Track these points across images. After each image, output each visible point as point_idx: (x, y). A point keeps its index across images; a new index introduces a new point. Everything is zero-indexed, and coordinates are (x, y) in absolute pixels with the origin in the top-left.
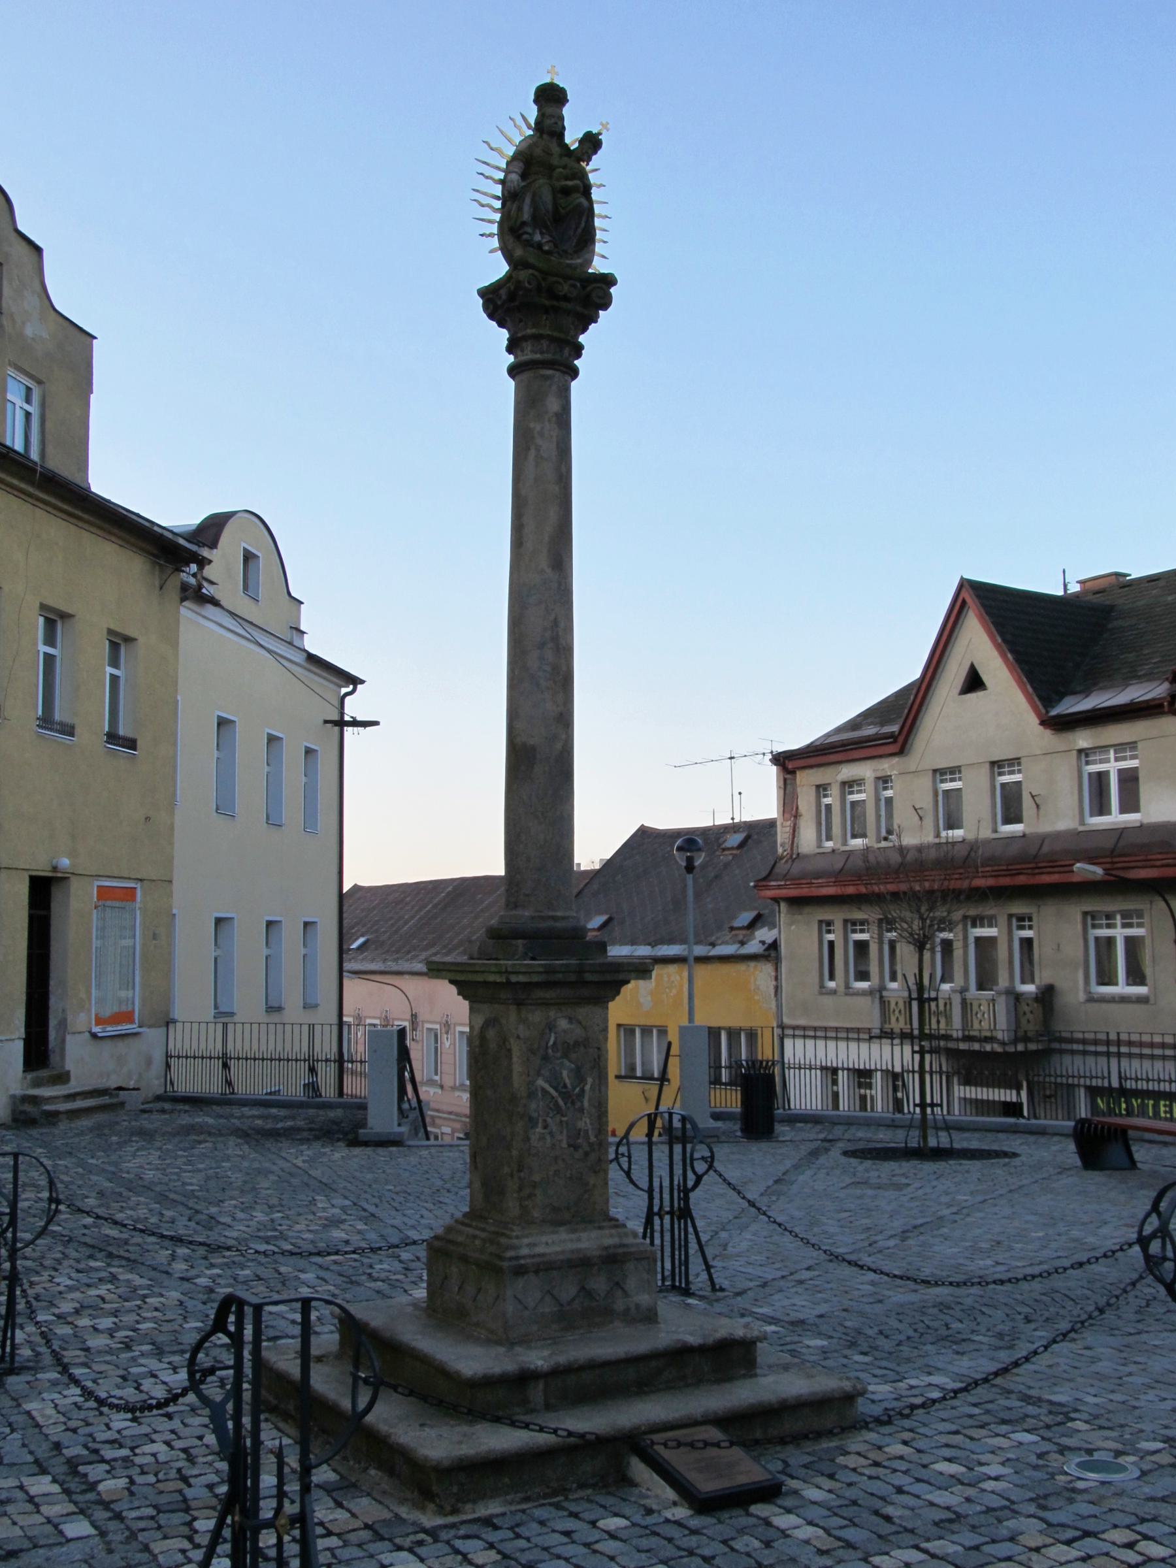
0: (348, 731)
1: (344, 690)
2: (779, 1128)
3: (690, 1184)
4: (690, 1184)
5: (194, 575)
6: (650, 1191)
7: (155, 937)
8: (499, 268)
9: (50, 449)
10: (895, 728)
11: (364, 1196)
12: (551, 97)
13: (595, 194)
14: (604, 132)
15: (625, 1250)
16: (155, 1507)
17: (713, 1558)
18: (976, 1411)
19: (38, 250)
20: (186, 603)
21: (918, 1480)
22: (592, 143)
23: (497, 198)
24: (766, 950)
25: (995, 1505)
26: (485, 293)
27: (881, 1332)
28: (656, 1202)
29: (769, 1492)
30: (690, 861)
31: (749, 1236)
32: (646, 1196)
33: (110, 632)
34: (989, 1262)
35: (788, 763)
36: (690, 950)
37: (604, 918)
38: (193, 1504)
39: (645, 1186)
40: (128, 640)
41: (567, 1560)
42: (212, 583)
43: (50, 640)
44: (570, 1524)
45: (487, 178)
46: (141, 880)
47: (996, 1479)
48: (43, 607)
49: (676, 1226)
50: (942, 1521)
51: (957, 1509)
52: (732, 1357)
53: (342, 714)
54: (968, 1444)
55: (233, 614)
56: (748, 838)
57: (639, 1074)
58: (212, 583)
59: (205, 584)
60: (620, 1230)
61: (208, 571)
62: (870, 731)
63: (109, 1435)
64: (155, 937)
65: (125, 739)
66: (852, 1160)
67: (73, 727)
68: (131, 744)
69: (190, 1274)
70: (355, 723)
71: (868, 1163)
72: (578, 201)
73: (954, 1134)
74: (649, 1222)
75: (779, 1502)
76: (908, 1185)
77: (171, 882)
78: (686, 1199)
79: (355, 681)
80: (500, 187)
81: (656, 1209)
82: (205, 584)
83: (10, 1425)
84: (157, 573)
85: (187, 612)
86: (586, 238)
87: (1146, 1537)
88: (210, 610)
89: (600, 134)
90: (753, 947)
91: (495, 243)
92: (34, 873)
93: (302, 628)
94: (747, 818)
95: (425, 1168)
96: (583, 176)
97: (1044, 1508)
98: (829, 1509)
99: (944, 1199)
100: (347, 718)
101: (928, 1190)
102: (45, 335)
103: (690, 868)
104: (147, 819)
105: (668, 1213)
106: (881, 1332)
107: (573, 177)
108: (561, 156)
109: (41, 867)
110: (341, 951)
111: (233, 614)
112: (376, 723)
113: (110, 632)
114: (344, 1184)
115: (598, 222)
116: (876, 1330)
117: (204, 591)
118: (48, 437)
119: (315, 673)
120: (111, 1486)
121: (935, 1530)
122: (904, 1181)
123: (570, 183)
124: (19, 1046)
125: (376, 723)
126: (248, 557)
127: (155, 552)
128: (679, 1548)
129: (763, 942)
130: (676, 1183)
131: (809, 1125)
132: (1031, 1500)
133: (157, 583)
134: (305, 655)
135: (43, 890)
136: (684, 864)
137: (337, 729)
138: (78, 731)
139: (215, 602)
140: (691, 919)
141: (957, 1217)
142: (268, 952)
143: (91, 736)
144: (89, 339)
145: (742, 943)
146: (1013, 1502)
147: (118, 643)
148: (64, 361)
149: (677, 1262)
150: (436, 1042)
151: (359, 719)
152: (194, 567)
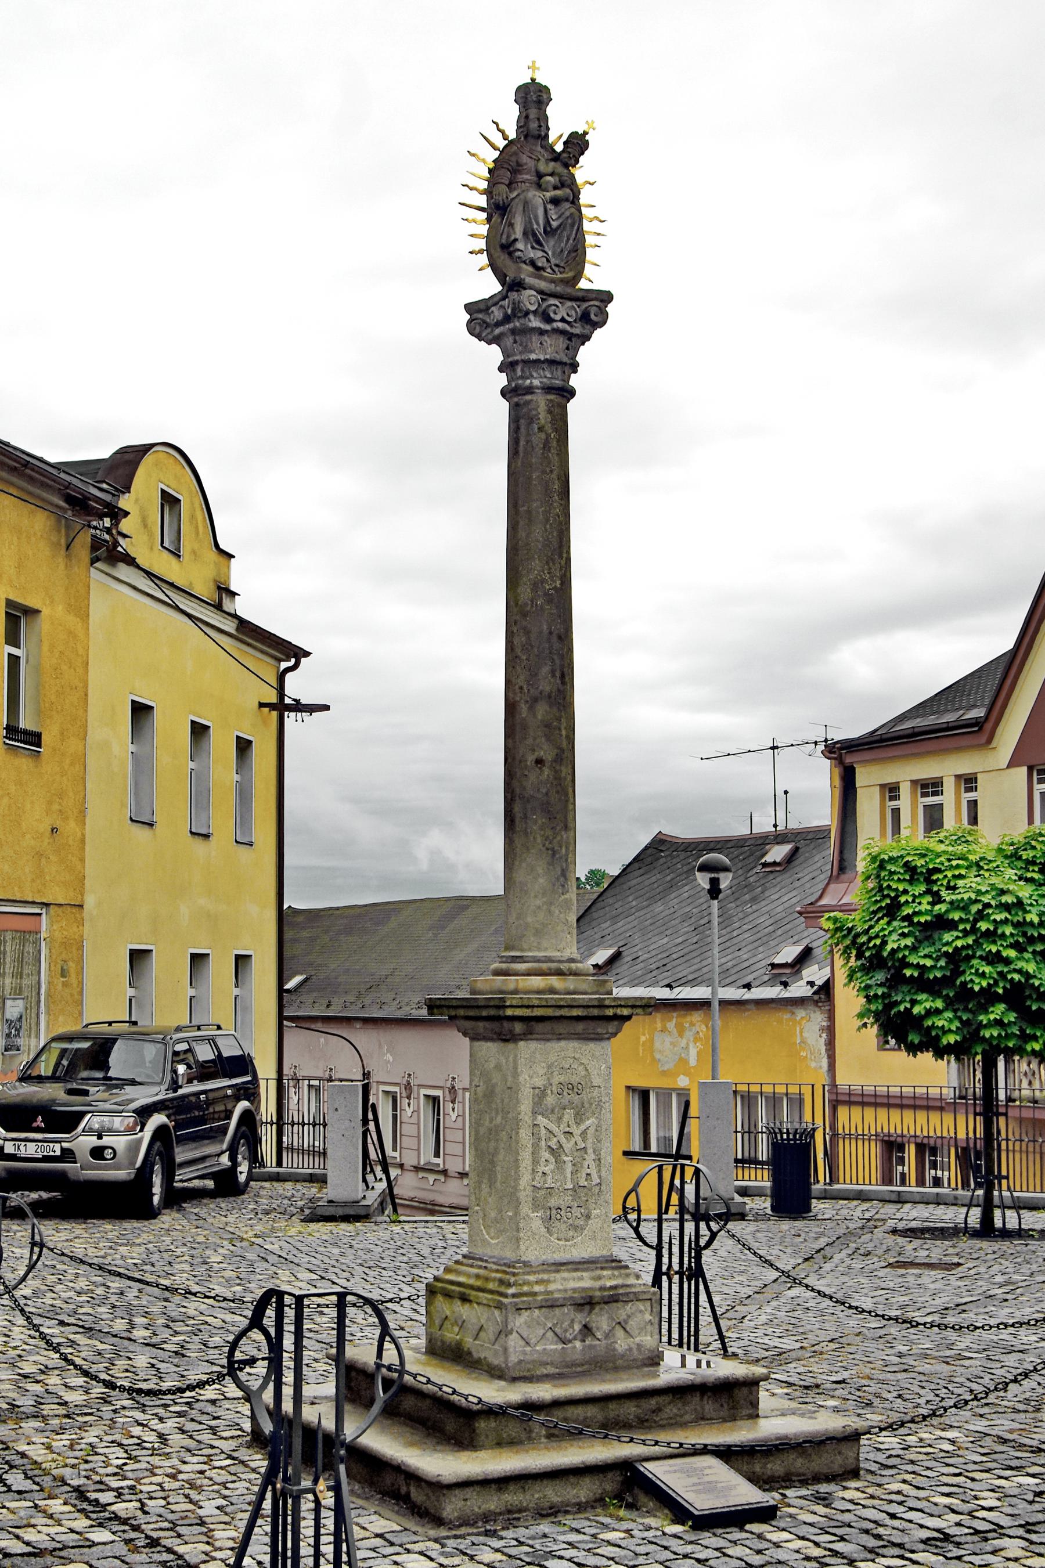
0: (291, 719)
1: (284, 665)
2: (816, 1205)
3: (703, 1242)
4: (703, 1242)
5: (108, 531)
6: (659, 1248)
7: (63, 973)
11: (332, 1269)
12: (533, 98)
13: (585, 197)
14: (591, 132)
15: (628, 1290)
16: (171, 1522)
17: (707, 1560)
18: (984, 1459)
21: (911, 1509)
22: (577, 144)
24: (814, 993)
25: (982, 1529)
28: (665, 1260)
29: (766, 1514)
30: (714, 883)
31: (769, 1311)
32: (654, 1252)
33: (10, 603)
35: (845, 755)
37: (610, 952)
38: (208, 1520)
39: (654, 1241)
40: (31, 612)
41: (570, 1560)
42: (125, 536)
46: (47, 905)
47: (990, 1509)
50: (929, 1539)
51: (946, 1531)
54: (969, 1484)
55: (149, 574)
56: (795, 851)
57: (654, 1149)
58: (125, 536)
59: (121, 540)
60: (623, 1271)
61: (125, 525)
63: (110, 1470)
68: (34, 739)
69: (154, 1340)
70: (298, 707)
73: (1024, 1213)
74: (657, 1282)
75: (773, 1523)
76: (959, 1265)
77: (81, 906)
78: (698, 1258)
79: (299, 654)
82: (121, 540)
83: (7, 1462)
86: (575, 256)
88: (123, 571)
89: (585, 133)
90: (799, 989)
91: (483, 259)
93: (233, 588)
95: (399, 1243)
97: (1028, 1531)
98: (821, 1529)
99: (999, 1279)
100: (287, 701)
101: (982, 1270)
105: (676, 1273)
106: (900, 1396)
110: (281, 991)
111: (149, 574)
112: (326, 708)
113: (10, 603)
114: (307, 1258)
116: (895, 1394)
117: (119, 549)
119: (249, 645)
120: (125, 1508)
122: (956, 1260)
125: (326, 708)
126: (169, 501)
128: (675, 1553)
129: (811, 984)
130: (686, 1239)
132: (1021, 1526)
133: (63, 541)
136: (708, 887)
140: (716, 958)
141: (1009, 1296)
142: (191, 992)
146: (1002, 1527)
150: (395, 1108)
151: (303, 702)
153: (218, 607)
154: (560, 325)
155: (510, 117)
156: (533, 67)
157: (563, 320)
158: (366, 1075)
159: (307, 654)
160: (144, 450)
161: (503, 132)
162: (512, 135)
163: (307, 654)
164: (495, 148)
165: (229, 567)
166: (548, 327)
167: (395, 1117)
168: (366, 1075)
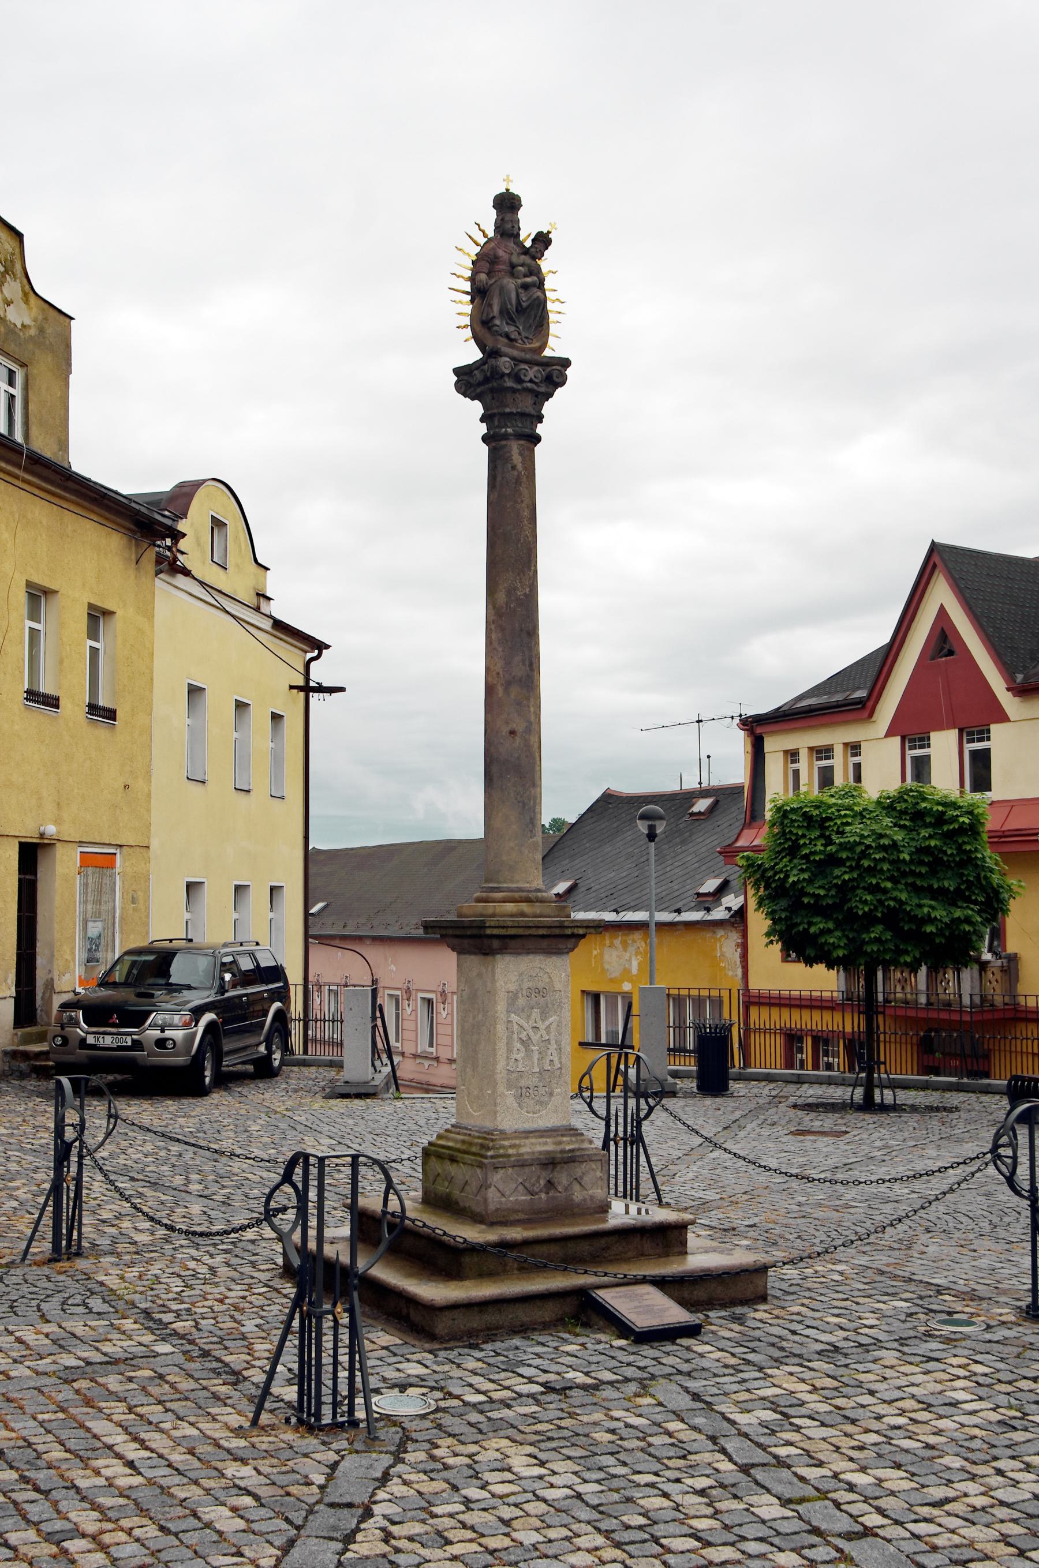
0: (314, 697)
3: (642, 1115)
4: (642, 1115)
5: (169, 549)
8: (473, 354)
9: (34, 431)
10: (862, 694)
11: (347, 1136)
12: (507, 205)
19: (19, 236)
20: (161, 576)
21: (808, 1327)
22: (543, 240)
23: (467, 293)
24: (731, 916)
26: (457, 371)
27: (799, 1237)
28: (613, 1129)
30: (652, 828)
32: (603, 1123)
33: (91, 606)
34: (906, 1191)
35: (757, 728)
36: (651, 916)
42: (183, 553)
43: (34, 616)
44: (539, 1349)
45: (458, 277)
46: (120, 846)
47: (871, 1327)
48: (29, 584)
49: (629, 1149)
50: (823, 1351)
52: (668, 1237)
53: (307, 678)
54: (855, 1307)
55: (202, 583)
57: (603, 1041)
58: (183, 553)
59: (179, 556)
61: (183, 545)
62: (823, 699)
63: (171, 1296)
64: (134, 901)
65: (104, 709)
66: (799, 1113)
67: (58, 699)
68: (110, 714)
70: (320, 689)
71: (813, 1115)
72: (535, 296)
74: (606, 1146)
76: (847, 1132)
79: (320, 646)
80: (469, 283)
81: (612, 1135)
82: (179, 556)
84: (133, 548)
85: (161, 584)
87: (976, 1362)
89: (549, 232)
90: (719, 914)
92: (23, 840)
93: (268, 595)
94: (715, 783)
96: (536, 272)
97: (902, 1345)
99: (878, 1144)
100: (312, 684)
102: (28, 321)
103: (652, 836)
104: (126, 787)
106: (799, 1237)
107: (531, 273)
108: (519, 254)
109: (29, 832)
111: (202, 583)
112: (342, 689)
113: (91, 606)
114: (327, 1128)
115: (550, 306)
118: (32, 418)
121: (817, 1356)
122: (844, 1129)
123: (528, 280)
124: (10, 1005)
125: (342, 689)
126: (217, 524)
127: (132, 527)
128: (621, 1362)
129: (729, 909)
130: (629, 1112)
131: (764, 1083)
132: (896, 1340)
133: (133, 557)
134: (272, 621)
135: (31, 855)
136: (646, 832)
137: (302, 694)
138: (62, 703)
139: (186, 572)
141: (886, 1158)
142: (235, 916)
143: (73, 707)
144: (68, 320)
145: (708, 910)
147: (97, 617)
148: (42, 344)
149: (629, 1187)
150: (397, 1008)
151: (325, 685)
152: (168, 542)
153: (257, 609)
154: (529, 385)
155: (489, 218)
156: (507, 180)
157: (531, 381)
158: (374, 982)
159: (328, 647)
160: (198, 484)
161: (483, 232)
162: (491, 233)
163: (328, 647)
164: (477, 244)
165: (265, 578)
166: (519, 387)
167: (397, 1015)
168: (374, 982)
